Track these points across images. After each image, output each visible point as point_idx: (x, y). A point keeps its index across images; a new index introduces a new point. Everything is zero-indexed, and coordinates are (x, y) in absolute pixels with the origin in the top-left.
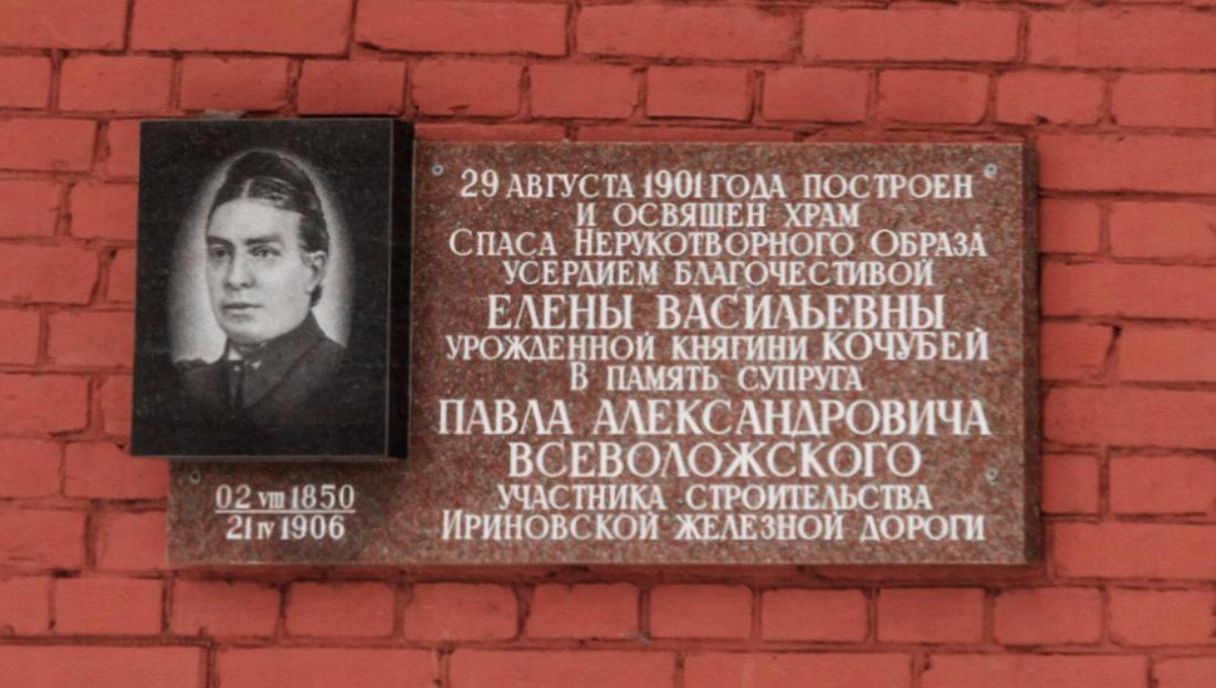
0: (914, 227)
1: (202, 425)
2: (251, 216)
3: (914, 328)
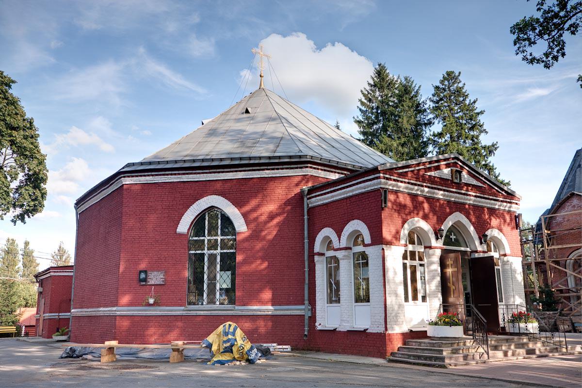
0: (210, 127)
1: (141, 280)
2: (142, 274)
3: (162, 277)
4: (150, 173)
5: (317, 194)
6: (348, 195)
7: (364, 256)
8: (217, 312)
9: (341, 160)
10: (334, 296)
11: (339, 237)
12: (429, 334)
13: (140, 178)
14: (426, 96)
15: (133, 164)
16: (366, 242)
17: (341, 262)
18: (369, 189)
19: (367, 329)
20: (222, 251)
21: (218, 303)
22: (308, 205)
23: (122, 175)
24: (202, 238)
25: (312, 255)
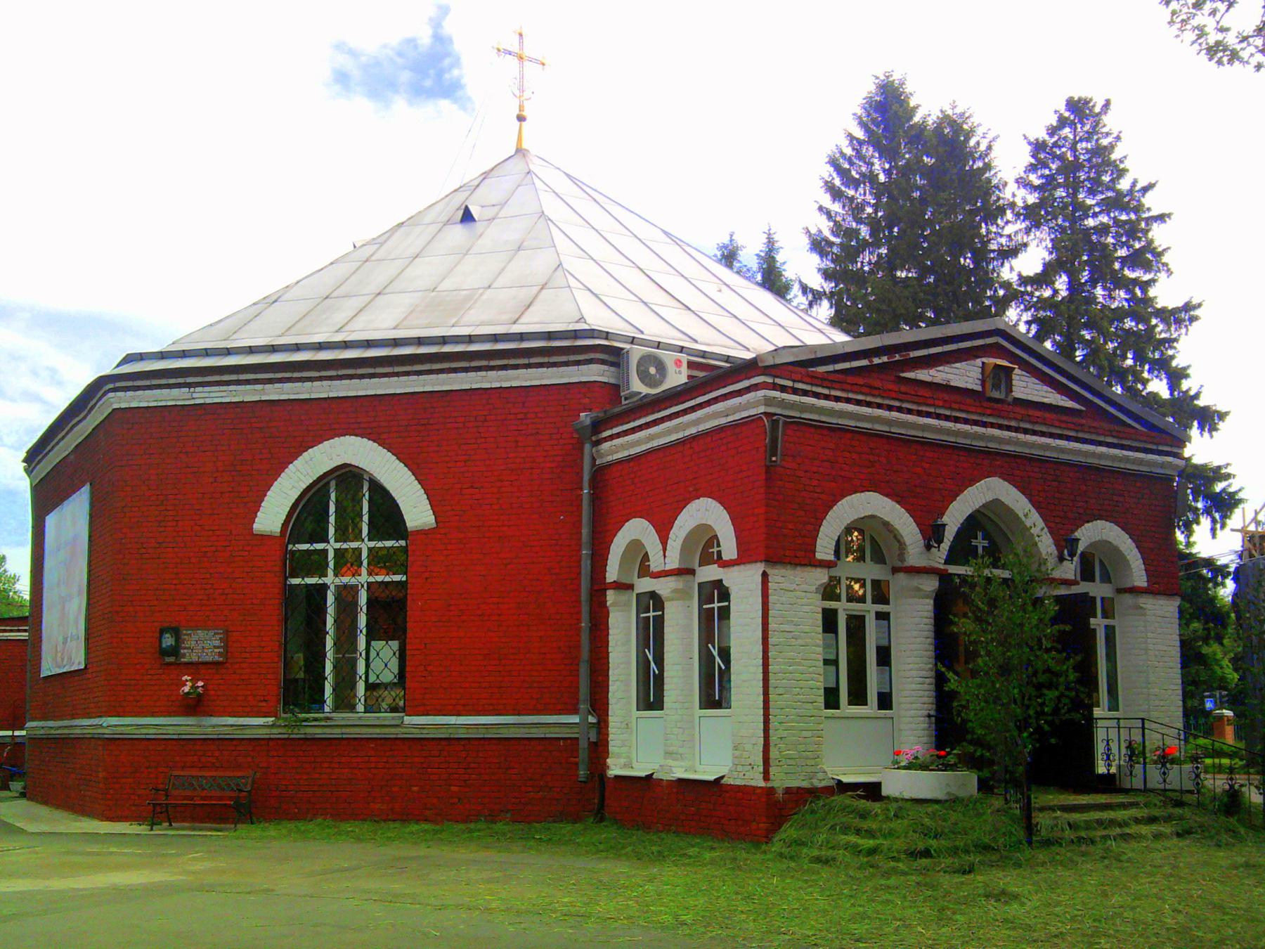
3: (217, 643)
4: (181, 380)
5: (616, 430)
6: (687, 433)
7: (720, 591)
8: (357, 730)
9: (696, 341)
10: (651, 696)
11: (664, 541)
12: (885, 792)
13: (158, 391)
14: (1009, 165)
15: (141, 357)
16: (725, 557)
17: (667, 604)
18: (737, 416)
19: (722, 777)
20: (371, 579)
21: (360, 708)
22: (594, 460)
23: (111, 386)
24: (354, 545)
25: (599, 588)
